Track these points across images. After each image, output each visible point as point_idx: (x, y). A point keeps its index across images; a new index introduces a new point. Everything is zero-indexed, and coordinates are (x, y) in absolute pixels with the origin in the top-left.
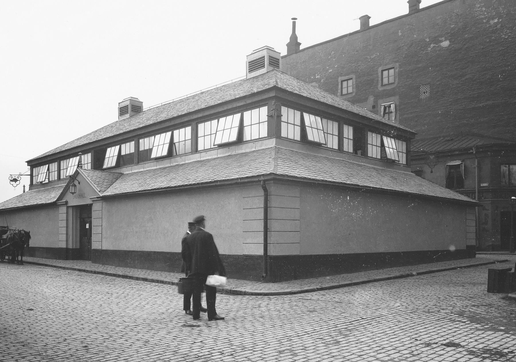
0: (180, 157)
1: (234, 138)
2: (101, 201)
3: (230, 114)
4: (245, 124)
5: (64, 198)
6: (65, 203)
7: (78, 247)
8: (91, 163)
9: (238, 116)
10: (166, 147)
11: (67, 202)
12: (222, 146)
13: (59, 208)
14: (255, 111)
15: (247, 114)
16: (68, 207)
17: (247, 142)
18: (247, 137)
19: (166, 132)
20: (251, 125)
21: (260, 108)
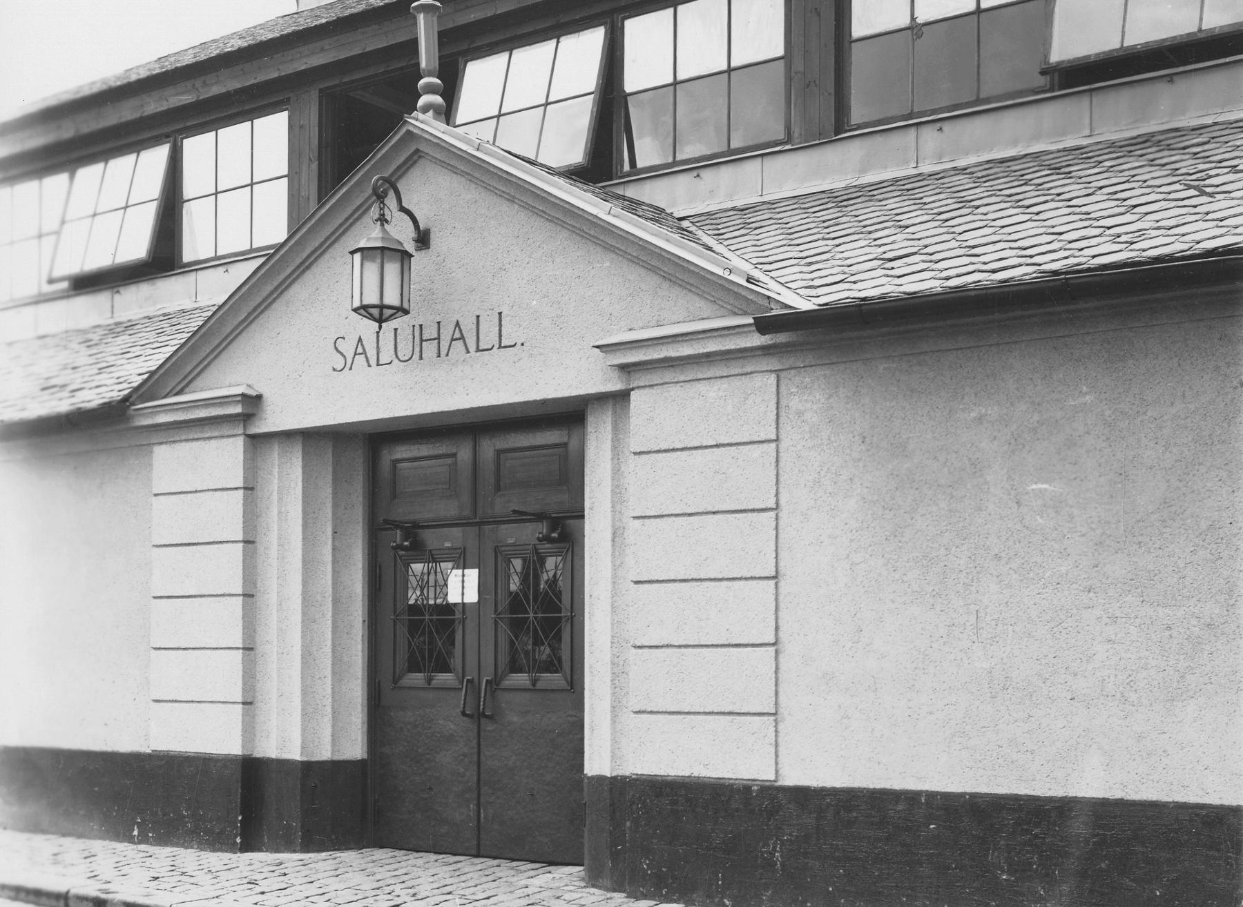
0: (222, 269)
1: (137, 247)
2: (774, 364)
3: (530, 34)
4: (189, 190)
5: (198, 383)
6: (238, 409)
7: (355, 748)
8: (293, 176)
9: (157, 157)
10: (582, 117)
11: (253, 403)
12: (86, 283)
13: (151, 452)
14: (234, 135)
15: (196, 148)
16: (257, 442)
17: (198, 266)
18: (195, 245)
19: (137, 146)
20: (216, 193)
21: (219, 131)
